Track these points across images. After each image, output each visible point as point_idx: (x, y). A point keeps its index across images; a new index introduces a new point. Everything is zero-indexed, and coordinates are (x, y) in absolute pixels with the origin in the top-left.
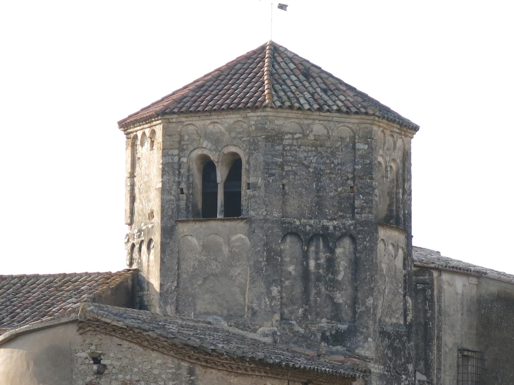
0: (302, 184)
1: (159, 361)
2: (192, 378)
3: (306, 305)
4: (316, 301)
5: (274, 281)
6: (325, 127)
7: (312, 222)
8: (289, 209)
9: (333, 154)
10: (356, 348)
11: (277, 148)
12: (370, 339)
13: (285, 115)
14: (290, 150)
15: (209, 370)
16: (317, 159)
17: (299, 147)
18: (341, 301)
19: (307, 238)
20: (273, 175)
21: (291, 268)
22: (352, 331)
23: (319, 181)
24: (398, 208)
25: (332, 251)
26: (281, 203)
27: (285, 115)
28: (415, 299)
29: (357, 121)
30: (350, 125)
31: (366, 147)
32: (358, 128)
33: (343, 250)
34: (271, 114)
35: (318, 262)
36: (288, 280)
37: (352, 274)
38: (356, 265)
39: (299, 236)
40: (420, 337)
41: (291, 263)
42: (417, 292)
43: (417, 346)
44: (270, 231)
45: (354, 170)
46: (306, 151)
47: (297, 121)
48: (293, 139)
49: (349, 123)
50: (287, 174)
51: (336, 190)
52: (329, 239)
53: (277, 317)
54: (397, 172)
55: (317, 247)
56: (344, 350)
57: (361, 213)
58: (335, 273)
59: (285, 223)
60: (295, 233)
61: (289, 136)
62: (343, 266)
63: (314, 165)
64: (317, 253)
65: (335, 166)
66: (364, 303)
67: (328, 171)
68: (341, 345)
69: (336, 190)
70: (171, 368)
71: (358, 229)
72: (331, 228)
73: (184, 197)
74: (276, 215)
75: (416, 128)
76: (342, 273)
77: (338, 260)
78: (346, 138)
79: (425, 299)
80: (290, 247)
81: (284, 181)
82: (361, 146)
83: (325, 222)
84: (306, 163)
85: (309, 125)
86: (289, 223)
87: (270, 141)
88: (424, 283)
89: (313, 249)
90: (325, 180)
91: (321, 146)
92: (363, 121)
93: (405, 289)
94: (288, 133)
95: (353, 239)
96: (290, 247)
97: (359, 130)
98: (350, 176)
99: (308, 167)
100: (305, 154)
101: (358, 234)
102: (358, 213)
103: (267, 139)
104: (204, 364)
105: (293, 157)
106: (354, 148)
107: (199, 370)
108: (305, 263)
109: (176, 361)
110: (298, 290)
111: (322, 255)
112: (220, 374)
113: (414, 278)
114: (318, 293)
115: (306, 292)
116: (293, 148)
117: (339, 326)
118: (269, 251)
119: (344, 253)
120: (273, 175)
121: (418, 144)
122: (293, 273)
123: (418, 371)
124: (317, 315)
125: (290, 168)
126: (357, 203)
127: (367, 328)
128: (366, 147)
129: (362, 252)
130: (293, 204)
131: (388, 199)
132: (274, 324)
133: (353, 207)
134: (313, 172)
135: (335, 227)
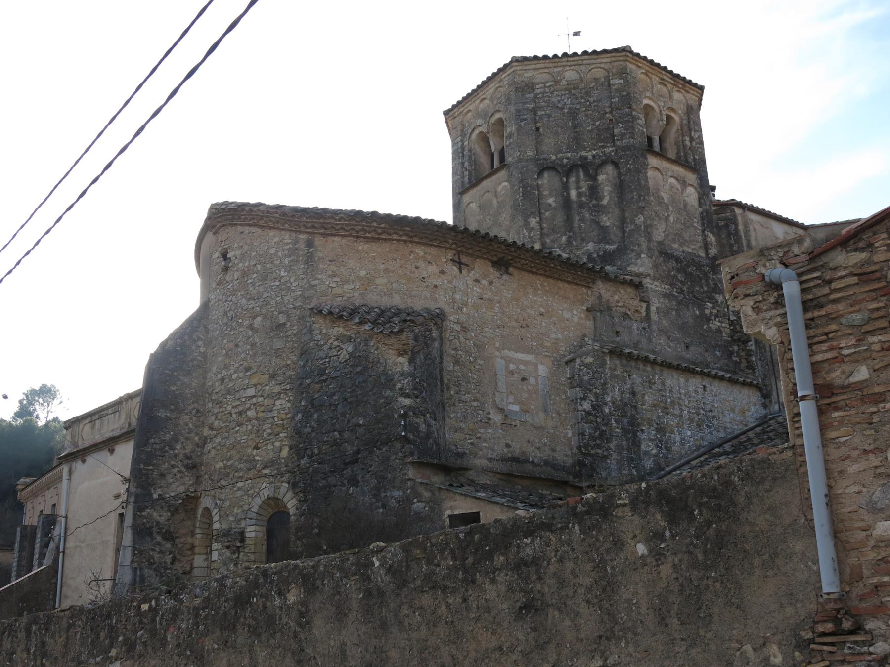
1: (276, 239)
2: (311, 250)
4: (580, 228)
5: (532, 213)
6: (577, 72)
7: (569, 154)
8: (544, 148)
10: (628, 265)
11: (528, 96)
12: (643, 256)
13: (533, 66)
14: (543, 97)
15: (331, 238)
17: (552, 93)
18: (608, 224)
19: (568, 170)
20: (525, 119)
21: (551, 200)
22: (622, 250)
23: (574, 118)
24: (686, 154)
25: (594, 178)
26: (535, 142)
27: (533, 66)
28: (718, 235)
29: (609, 60)
30: (603, 65)
31: (622, 81)
33: (606, 177)
34: (518, 68)
37: (619, 197)
38: (621, 187)
39: (556, 170)
41: (551, 195)
42: (719, 228)
45: (611, 103)
47: (546, 70)
48: (545, 87)
50: (541, 118)
52: (591, 169)
54: (681, 123)
55: (578, 178)
57: (622, 140)
58: (599, 198)
59: (540, 160)
60: (545, 167)
61: (541, 85)
62: (607, 195)
64: (578, 182)
65: (591, 104)
66: (633, 222)
68: (610, 264)
69: (594, 125)
70: (288, 243)
72: (590, 157)
73: (467, 173)
74: (529, 153)
76: (607, 198)
79: (729, 234)
80: (549, 181)
81: (538, 125)
82: (617, 82)
83: (583, 153)
85: (559, 72)
86: (545, 159)
88: (726, 219)
89: (573, 179)
90: (581, 117)
91: (574, 89)
92: (614, 59)
93: (703, 225)
94: (539, 83)
95: (616, 164)
96: (548, 180)
98: (608, 110)
99: (562, 109)
102: (618, 140)
103: (517, 90)
104: (322, 231)
106: (609, 85)
107: (318, 241)
109: (294, 235)
110: (560, 219)
111: (582, 183)
112: (344, 241)
113: (715, 217)
114: (582, 220)
115: (569, 220)
117: (607, 246)
118: (524, 187)
119: (607, 179)
120: (525, 119)
122: (553, 204)
124: (583, 240)
126: (616, 131)
127: (639, 245)
128: (622, 81)
129: (626, 175)
130: (549, 143)
131: (675, 147)
133: (613, 135)
135: (594, 156)
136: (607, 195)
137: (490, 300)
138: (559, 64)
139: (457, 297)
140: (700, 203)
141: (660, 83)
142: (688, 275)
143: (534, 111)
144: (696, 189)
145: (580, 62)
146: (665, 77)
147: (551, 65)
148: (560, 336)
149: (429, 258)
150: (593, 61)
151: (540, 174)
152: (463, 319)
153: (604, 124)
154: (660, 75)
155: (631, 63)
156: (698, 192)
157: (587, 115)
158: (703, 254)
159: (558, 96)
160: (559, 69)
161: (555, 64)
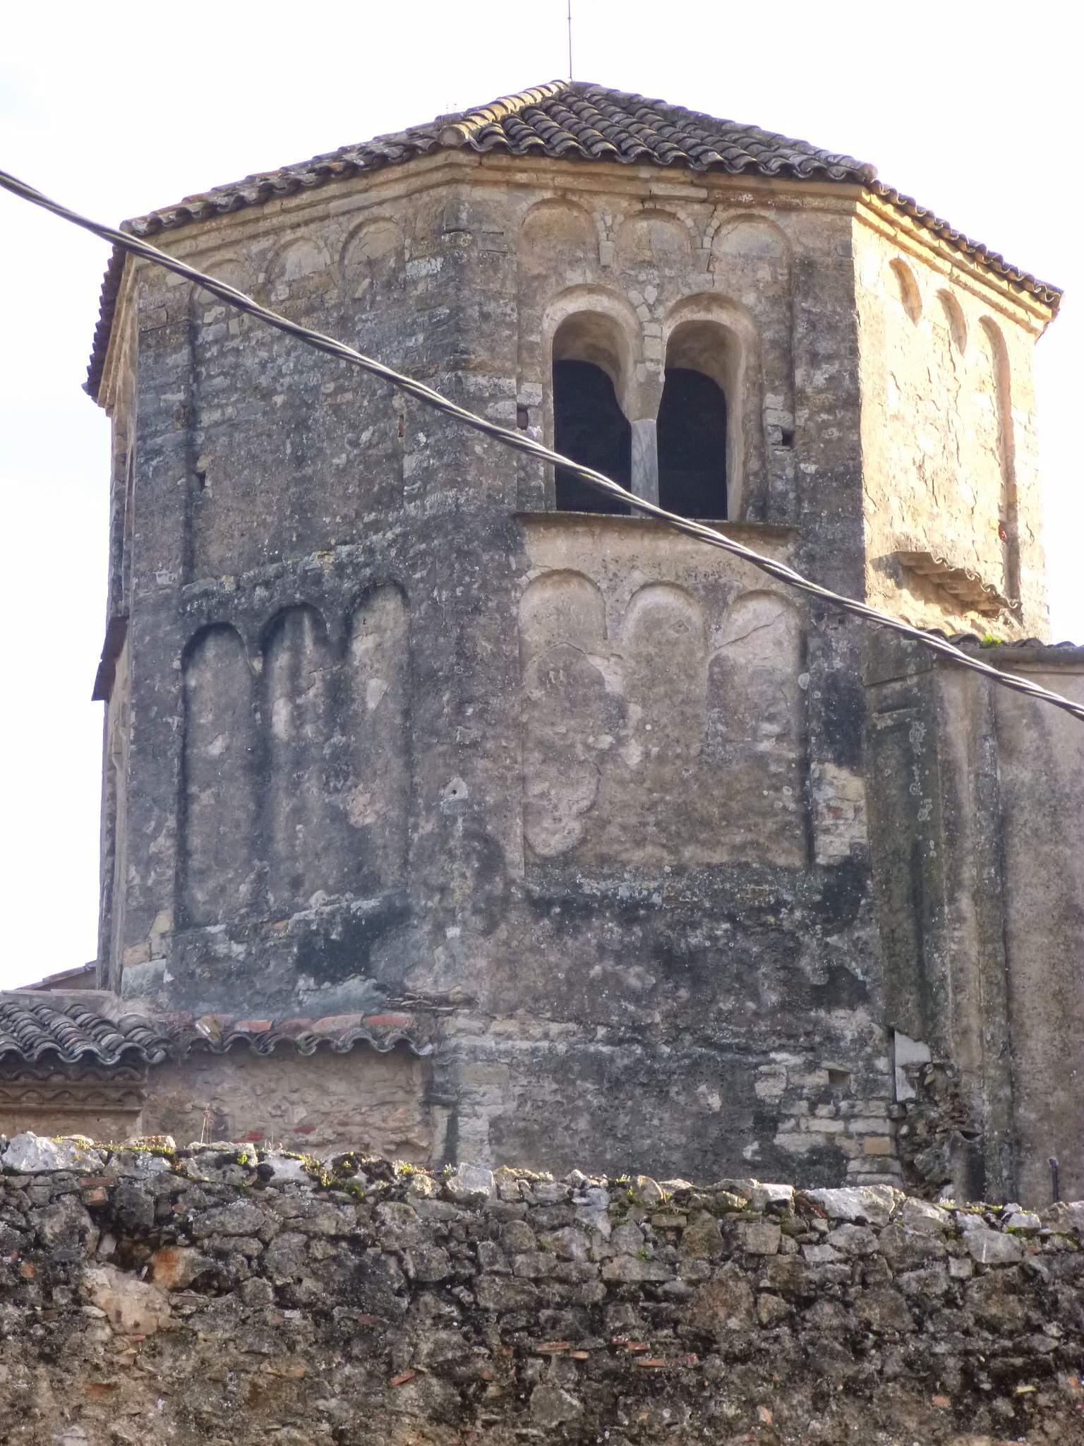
0: (253, 457)
3: (261, 860)
14: (222, 354)
16: (298, 358)
25: (342, 650)
29: (399, 189)
31: (437, 264)
32: (411, 211)
33: (378, 635)
35: (299, 701)
36: (209, 786)
38: (415, 678)
40: (897, 904)
41: (218, 727)
43: (890, 939)
44: (147, 639)
46: (263, 344)
47: (228, 254)
49: (381, 203)
51: (355, 443)
53: (164, 922)
55: (297, 651)
56: (367, 991)
57: (420, 495)
63: (286, 381)
67: (330, 387)
69: (355, 443)
71: (411, 553)
74: (163, 579)
77: (362, 677)
78: (385, 257)
79: (909, 758)
84: (264, 381)
86: (206, 594)
87: (149, 346)
89: (282, 660)
92: (416, 183)
97: (415, 214)
99: (267, 395)
100: (264, 354)
101: (413, 567)
105: (225, 374)
108: (258, 716)
116: (230, 344)
120: (158, 452)
123: (901, 1032)
125: (217, 415)
128: (437, 264)
132: (154, 950)
134: (284, 405)
138: (264, 225)
140: (804, 655)
141: (645, 214)
142: (670, 961)
143: (190, 416)
145: (320, 210)
146: (657, 189)
147: (235, 234)
150: (358, 200)
153: (384, 434)
154: (630, 188)
155: (476, 183)
156: (798, 611)
157: (336, 409)
158: (787, 857)
159: (261, 344)
160: (264, 243)
161: (250, 229)
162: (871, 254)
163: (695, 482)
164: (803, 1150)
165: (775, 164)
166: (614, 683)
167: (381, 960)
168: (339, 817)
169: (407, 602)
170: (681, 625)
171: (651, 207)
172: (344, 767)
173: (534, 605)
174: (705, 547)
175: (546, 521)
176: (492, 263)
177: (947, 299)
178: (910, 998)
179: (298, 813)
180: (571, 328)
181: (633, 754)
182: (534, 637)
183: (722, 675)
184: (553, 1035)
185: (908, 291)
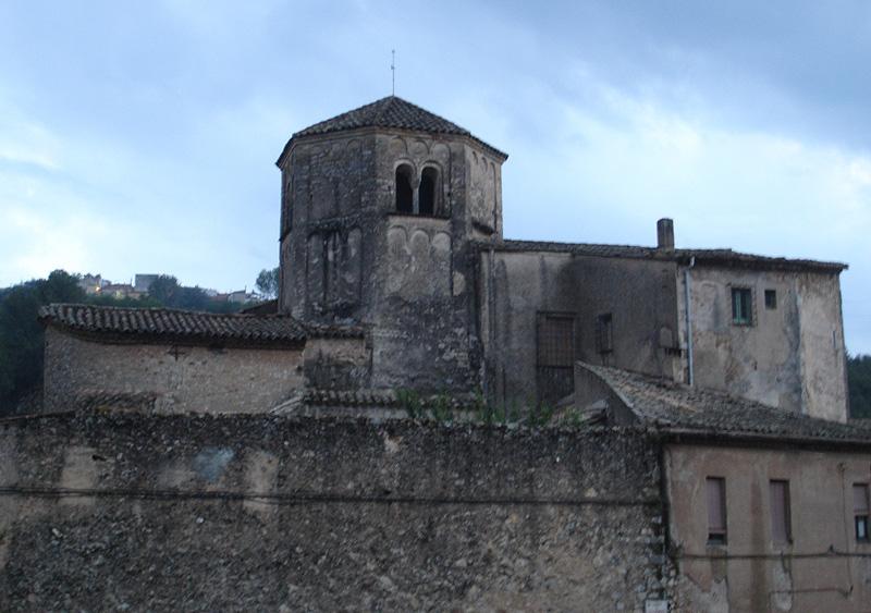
9: (347, 164)
25: (345, 242)
31: (370, 152)
33: (354, 238)
55: (335, 239)
57: (365, 207)
75: (506, 157)
79: (475, 271)
89: (331, 242)
121: (505, 167)
136: (353, 252)
137: (202, 376)
139: (173, 378)
140: (452, 248)
144: (448, 234)
148: (268, 393)
149: (151, 353)
151: (309, 238)
152: (177, 393)
158: (448, 293)
162: (469, 151)
163: (427, 210)
164: (251, 287)
165: (448, 130)
166: (409, 252)
167: (355, 315)
168: (344, 280)
169: (362, 232)
170: (424, 239)
171: (419, 140)
172: (345, 269)
173: (391, 233)
174: (430, 222)
175: (394, 214)
176: (383, 152)
177: (483, 159)
178: (473, 327)
179: (335, 279)
180: (400, 167)
181: (413, 269)
182: (390, 241)
183: (433, 251)
184: (395, 333)
185: (485, 162)
